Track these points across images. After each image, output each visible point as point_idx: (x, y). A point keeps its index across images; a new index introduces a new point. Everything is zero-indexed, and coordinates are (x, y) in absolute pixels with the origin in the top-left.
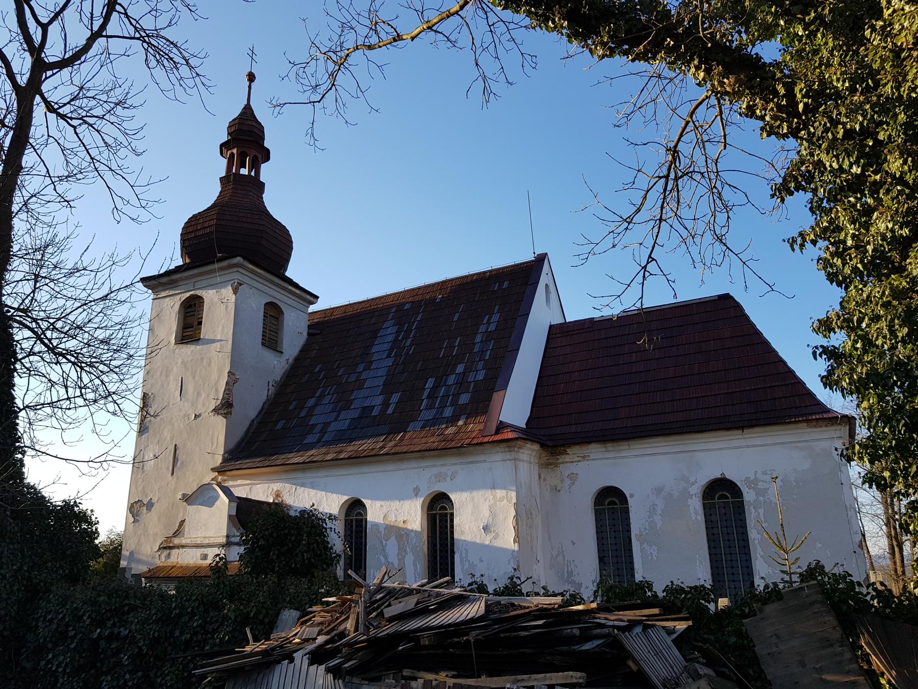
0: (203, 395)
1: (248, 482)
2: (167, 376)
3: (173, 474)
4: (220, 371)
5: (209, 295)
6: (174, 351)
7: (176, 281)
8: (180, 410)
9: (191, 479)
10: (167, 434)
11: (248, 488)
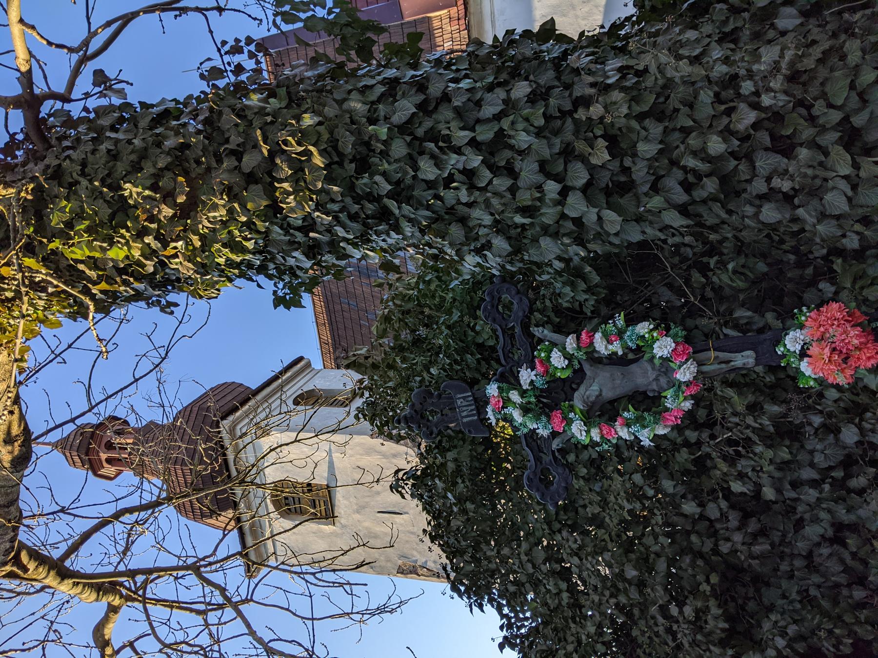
4: (369, 451)
6: (344, 526)
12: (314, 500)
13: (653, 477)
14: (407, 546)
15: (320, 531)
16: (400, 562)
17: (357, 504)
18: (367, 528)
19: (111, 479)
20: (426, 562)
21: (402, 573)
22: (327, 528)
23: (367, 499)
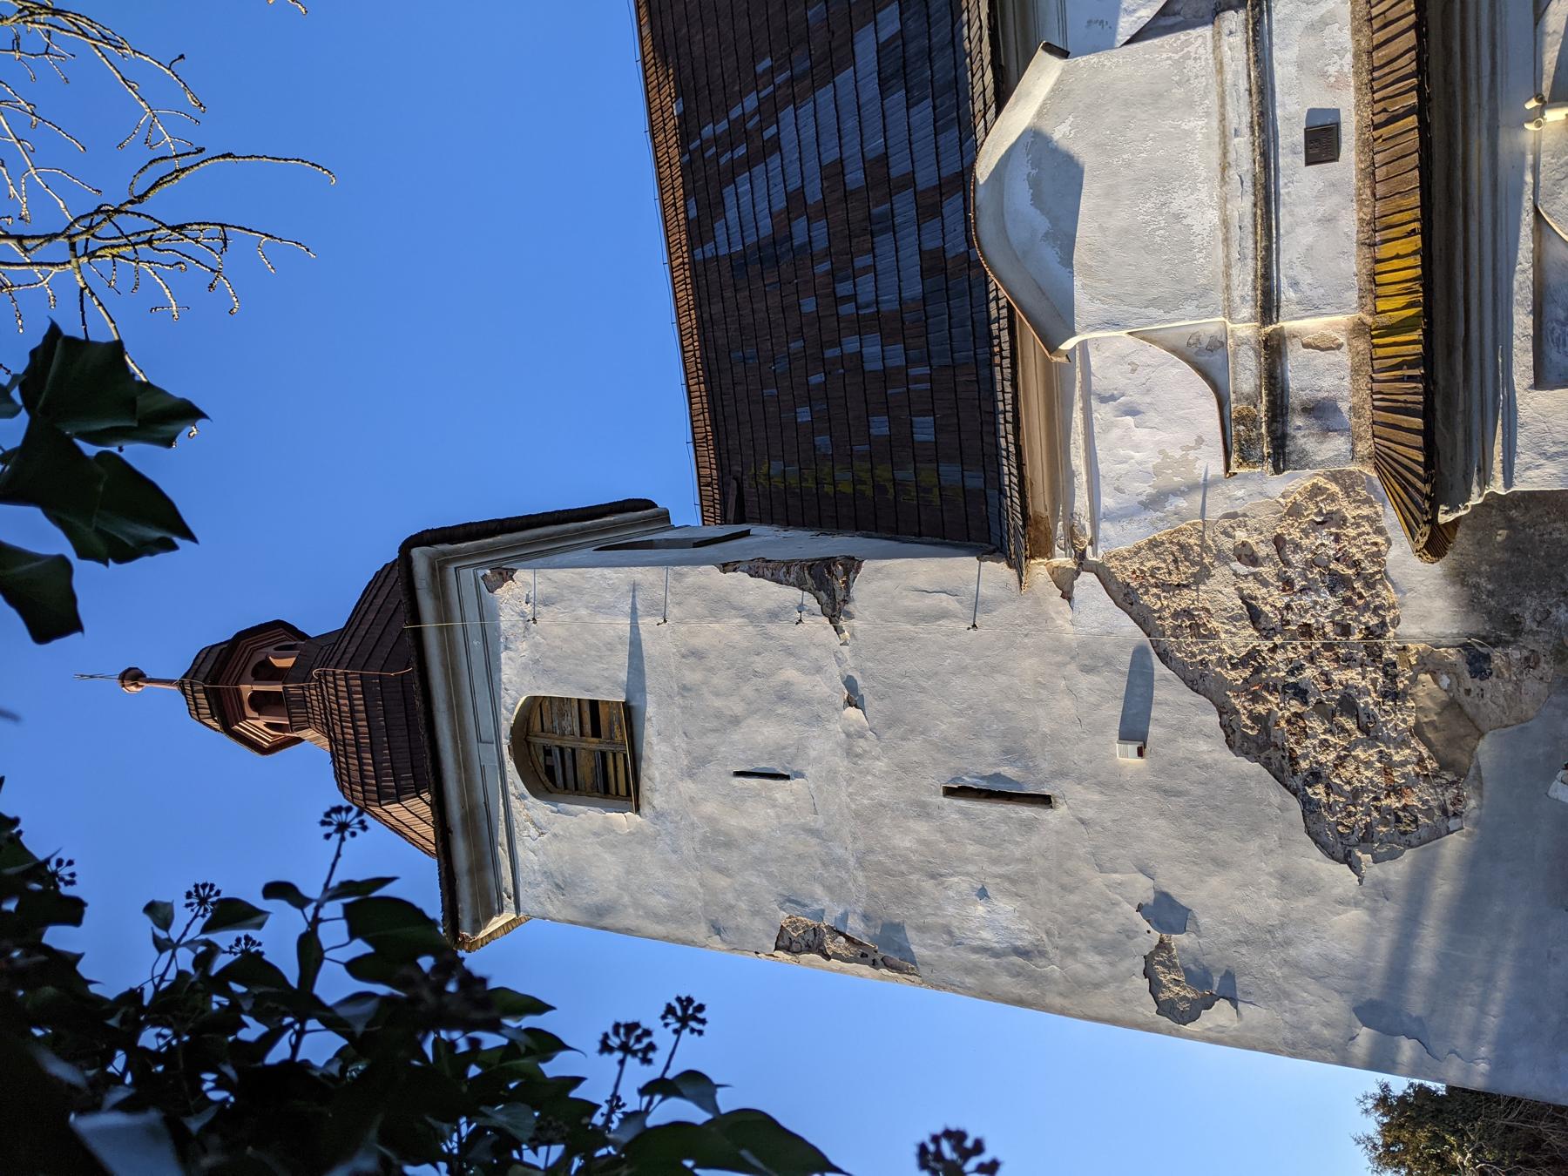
0: (790, 674)
1: (1077, 417)
2: (729, 844)
3: (1045, 801)
4: (719, 606)
5: (517, 683)
6: (659, 815)
7: (470, 817)
8: (832, 776)
9: (1067, 702)
10: (908, 837)
11: (1101, 412)
12: (604, 754)
13: (771, 253)
14: (801, 869)
15: (610, 829)
16: (783, 917)
17: (689, 753)
18: (711, 820)
19: (264, 751)
20: (845, 917)
21: (788, 950)
22: (623, 820)
23: (711, 739)
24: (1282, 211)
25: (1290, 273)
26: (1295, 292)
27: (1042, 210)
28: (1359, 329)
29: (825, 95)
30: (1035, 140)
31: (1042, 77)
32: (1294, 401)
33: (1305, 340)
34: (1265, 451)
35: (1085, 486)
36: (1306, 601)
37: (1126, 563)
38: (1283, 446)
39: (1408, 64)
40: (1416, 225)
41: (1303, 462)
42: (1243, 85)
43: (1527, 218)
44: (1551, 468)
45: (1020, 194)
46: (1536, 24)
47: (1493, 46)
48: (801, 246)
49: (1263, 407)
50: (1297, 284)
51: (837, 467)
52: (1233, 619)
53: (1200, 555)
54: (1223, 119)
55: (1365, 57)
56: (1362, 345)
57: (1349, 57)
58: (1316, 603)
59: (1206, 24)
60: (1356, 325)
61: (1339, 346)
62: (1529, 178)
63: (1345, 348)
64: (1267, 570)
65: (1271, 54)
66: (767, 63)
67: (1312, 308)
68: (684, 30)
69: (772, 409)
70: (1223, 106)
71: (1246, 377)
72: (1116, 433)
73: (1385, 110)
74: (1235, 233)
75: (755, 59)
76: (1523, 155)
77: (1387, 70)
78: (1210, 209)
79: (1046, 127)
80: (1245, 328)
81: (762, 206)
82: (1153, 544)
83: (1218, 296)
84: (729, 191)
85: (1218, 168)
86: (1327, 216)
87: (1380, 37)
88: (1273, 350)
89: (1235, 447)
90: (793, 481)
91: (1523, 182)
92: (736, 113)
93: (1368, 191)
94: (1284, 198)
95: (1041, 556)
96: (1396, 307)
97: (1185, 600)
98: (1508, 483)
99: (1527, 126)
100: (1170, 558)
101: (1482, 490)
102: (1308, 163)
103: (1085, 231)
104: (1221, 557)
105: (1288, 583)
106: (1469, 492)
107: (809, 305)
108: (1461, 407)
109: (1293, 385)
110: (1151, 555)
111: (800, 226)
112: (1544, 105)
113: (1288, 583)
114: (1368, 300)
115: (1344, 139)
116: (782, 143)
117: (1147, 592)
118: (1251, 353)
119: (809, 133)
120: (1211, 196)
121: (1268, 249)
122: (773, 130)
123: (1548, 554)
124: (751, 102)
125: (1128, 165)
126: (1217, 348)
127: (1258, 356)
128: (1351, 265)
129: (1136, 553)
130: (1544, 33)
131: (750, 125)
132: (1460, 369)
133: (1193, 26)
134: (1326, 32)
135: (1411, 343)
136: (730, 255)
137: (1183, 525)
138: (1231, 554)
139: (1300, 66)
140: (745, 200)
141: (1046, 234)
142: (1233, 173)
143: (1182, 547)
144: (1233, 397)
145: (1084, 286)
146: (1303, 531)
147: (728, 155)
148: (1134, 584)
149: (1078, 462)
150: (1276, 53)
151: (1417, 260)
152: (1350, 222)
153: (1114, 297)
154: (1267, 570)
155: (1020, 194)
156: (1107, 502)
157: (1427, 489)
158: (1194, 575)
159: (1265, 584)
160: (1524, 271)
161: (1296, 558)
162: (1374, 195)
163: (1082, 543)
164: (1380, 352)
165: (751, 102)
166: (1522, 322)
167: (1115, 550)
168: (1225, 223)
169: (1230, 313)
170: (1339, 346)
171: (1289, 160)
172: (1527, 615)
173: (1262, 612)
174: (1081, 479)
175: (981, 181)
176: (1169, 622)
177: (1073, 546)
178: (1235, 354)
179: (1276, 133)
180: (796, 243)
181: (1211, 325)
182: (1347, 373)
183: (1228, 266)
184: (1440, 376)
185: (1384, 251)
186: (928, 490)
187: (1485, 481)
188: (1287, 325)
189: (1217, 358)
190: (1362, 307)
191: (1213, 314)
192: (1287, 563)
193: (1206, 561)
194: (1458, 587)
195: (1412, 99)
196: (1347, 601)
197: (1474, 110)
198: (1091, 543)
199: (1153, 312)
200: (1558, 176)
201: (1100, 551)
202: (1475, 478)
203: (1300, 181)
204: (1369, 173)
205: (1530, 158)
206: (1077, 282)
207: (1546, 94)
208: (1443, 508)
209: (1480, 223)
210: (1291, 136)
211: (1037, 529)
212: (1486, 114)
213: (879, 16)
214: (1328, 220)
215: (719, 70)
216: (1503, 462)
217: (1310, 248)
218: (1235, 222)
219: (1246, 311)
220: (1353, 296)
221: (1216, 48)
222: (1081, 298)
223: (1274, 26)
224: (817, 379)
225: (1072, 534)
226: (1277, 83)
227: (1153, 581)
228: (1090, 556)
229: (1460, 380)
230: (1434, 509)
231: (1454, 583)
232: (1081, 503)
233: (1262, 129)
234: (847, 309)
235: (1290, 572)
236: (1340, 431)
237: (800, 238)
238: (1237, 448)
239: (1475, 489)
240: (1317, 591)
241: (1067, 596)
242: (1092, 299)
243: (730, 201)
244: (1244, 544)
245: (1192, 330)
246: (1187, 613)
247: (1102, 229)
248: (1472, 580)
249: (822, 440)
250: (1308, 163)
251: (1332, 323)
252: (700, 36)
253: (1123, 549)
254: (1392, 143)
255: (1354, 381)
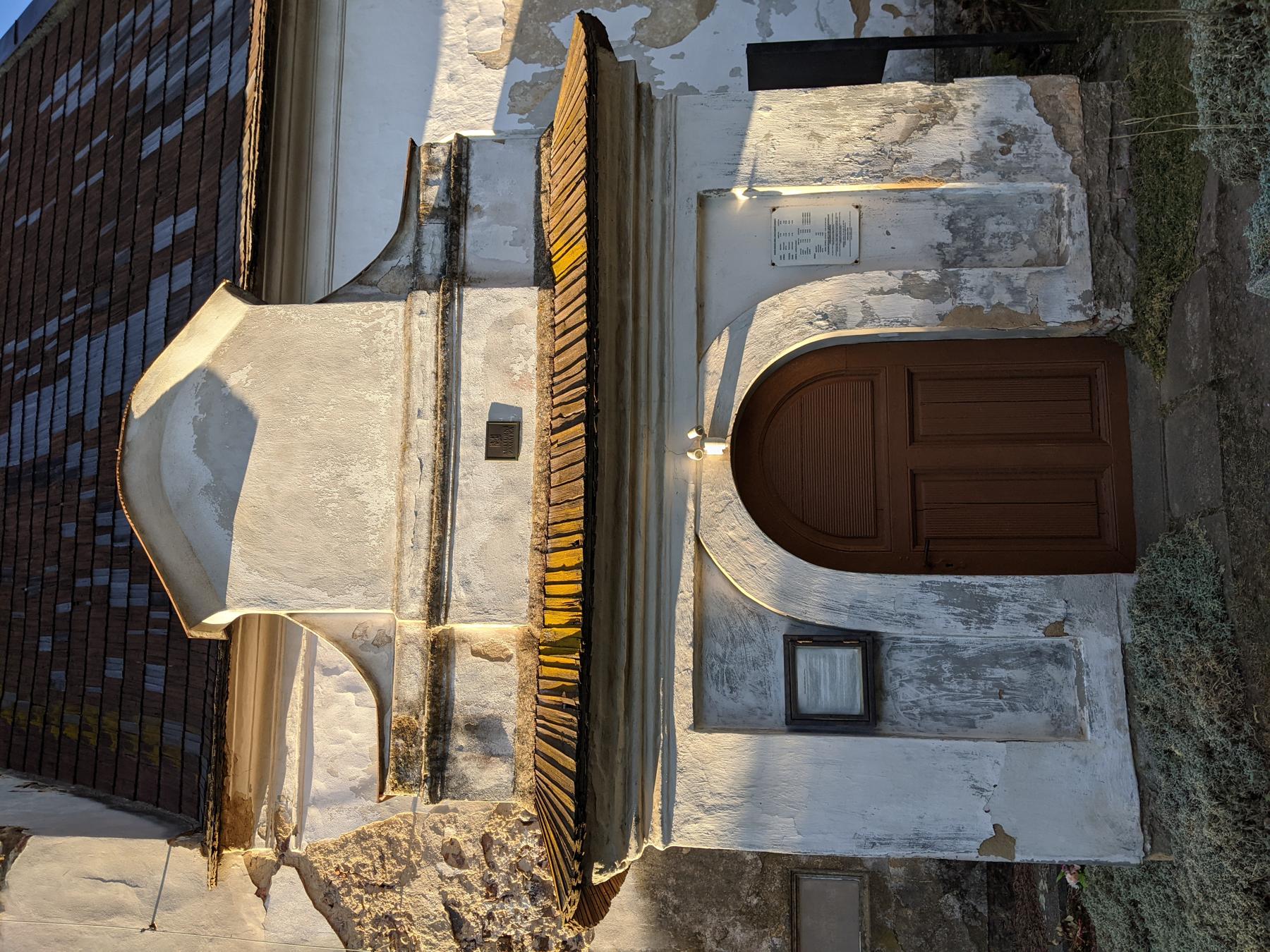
1: (298, 687)
24: (459, 502)
25: (463, 570)
26: (466, 591)
27: (205, 460)
28: (529, 642)
29: (117, 331)
30: (206, 382)
31: (221, 318)
32: (459, 716)
33: (476, 646)
34: (424, 773)
35: (296, 765)
36: (508, 909)
37: (331, 857)
38: (442, 769)
39: (579, 372)
40: (579, 537)
41: (463, 792)
42: (430, 367)
43: (689, 547)
44: (709, 823)
45: (182, 435)
46: (699, 362)
47: (662, 374)
48: (73, 470)
49: (424, 719)
50: (468, 583)
51: (68, 707)
52: (435, 928)
53: (407, 852)
54: (407, 398)
55: (547, 361)
56: (530, 659)
57: (533, 359)
58: (517, 912)
59: (399, 299)
60: (526, 636)
61: (509, 658)
62: (691, 506)
63: (514, 661)
64: (472, 873)
65: (459, 341)
66: (72, 293)
67: (482, 612)
68: (8, 252)
69: (17, 633)
70: (408, 384)
71: (410, 684)
72: (336, 709)
73: (561, 416)
74: (410, 516)
75: (62, 289)
76: (686, 482)
77: (564, 376)
78: (388, 489)
79: (222, 370)
80: (414, 627)
81: (45, 425)
82: (361, 837)
83: (387, 585)
84: (17, 406)
85: (400, 448)
86: (507, 521)
87: (560, 343)
88: (441, 653)
89: (392, 765)
90: (22, 716)
91: (685, 510)
92: (38, 334)
93: (543, 496)
94: (462, 489)
95: (235, 846)
96: (562, 623)
97: (386, 903)
98: (667, 838)
99: (689, 455)
100: (377, 854)
101: (640, 844)
102: (488, 457)
103: (251, 491)
104: (428, 856)
105: (492, 888)
106: (626, 846)
107: (69, 530)
108: (621, 744)
109: (459, 697)
110: (357, 849)
111: (75, 449)
112: (703, 437)
113: (492, 888)
114: (537, 611)
115: (524, 439)
116: (73, 369)
117: (348, 893)
118: (418, 654)
119: (97, 363)
120: (390, 475)
121: (441, 540)
122: (66, 355)
123: (726, 871)
124: (52, 326)
125: (306, 427)
126: (384, 643)
127: (425, 658)
128: (524, 571)
129: (342, 847)
130: (705, 372)
131: (48, 347)
132: (621, 700)
133: (388, 299)
134: (514, 331)
135: (567, 669)
136: (7, 469)
137: (394, 817)
138: (438, 853)
139: (487, 358)
140: (31, 417)
141: (207, 488)
142: (413, 456)
143: (390, 842)
144: (395, 703)
145: (243, 553)
146: (510, 831)
147: (23, 372)
148: (336, 883)
149: (293, 738)
150: (464, 342)
151: (577, 575)
152: (525, 524)
153: (277, 570)
154: (472, 873)
155: (182, 435)
156: (319, 784)
157: (576, 846)
158: (399, 875)
159: (469, 888)
160: (685, 600)
161: (501, 861)
162: (549, 500)
163: (286, 831)
164: (546, 671)
165: (52, 326)
166: (683, 654)
167: (320, 841)
168: (402, 507)
169: (398, 607)
170: (509, 658)
171: (469, 450)
172: (708, 934)
173: (464, 920)
174: (294, 758)
175: (137, 415)
176: (368, 930)
177: (276, 834)
178: (401, 653)
179: (458, 420)
180: (69, 466)
181: (381, 617)
182: (514, 688)
183: (400, 554)
184: (600, 706)
185: (555, 560)
186: (150, 749)
187: (643, 835)
188: (459, 628)
189: (383, 654)
190: (532, 616)
191: (380, 605)
192: (492, 866)
193: (413, 859)
194: (648, 900)
195: (581, 407)
196: (547, 912)
197: (643, 431)
198: (295, 833)
199: (316, 593)
200: (716, 509)
201: (304, 843)
202: (633, 829)
203: (478, 474)
204: (546, 477)
205: (692, 487)
206: (236, 547)
207: (707, 429)
208: (597, 866)
209: (646, 544)
210: (473, 429)
211: (236, 813)
212: (654, 437)
213: (175, 269)
214: (504, 520)
215: (30, 293)
216: (662, 812)
217: (484, 546)
218: (411, 506)
219: (417, 606)
220: (524, 603)
221: (407, 325)
222: (237, 565)
223: (465, 314)
224: (64, 608)
225: (277, 819)
226: (463, 371)
227: (356, 880)
228: (293, 848)
229: (621, 713)
230: (586, 870)
231: (644, 896)
232: (290, 785)
233: (445, 415)
234: (103, 540)
235: (496, 877)
236: (505, 756)
237: (72, 463)
238: (391, 768)
239: (633, 843)
240: (519, 899)
241: (262, 894)
242: (249, 570)
243: (17, 417)
244: (452, 842)
245: (360, 619)
246: (389, 919)
247: (271, 492)
248: (661, 893)
249: (58, 675)
250: (488, 457)
251: (501, 631)
252: (20, 260)
253: (328, 841)
254: (565, 448)
255: (521, 699)
